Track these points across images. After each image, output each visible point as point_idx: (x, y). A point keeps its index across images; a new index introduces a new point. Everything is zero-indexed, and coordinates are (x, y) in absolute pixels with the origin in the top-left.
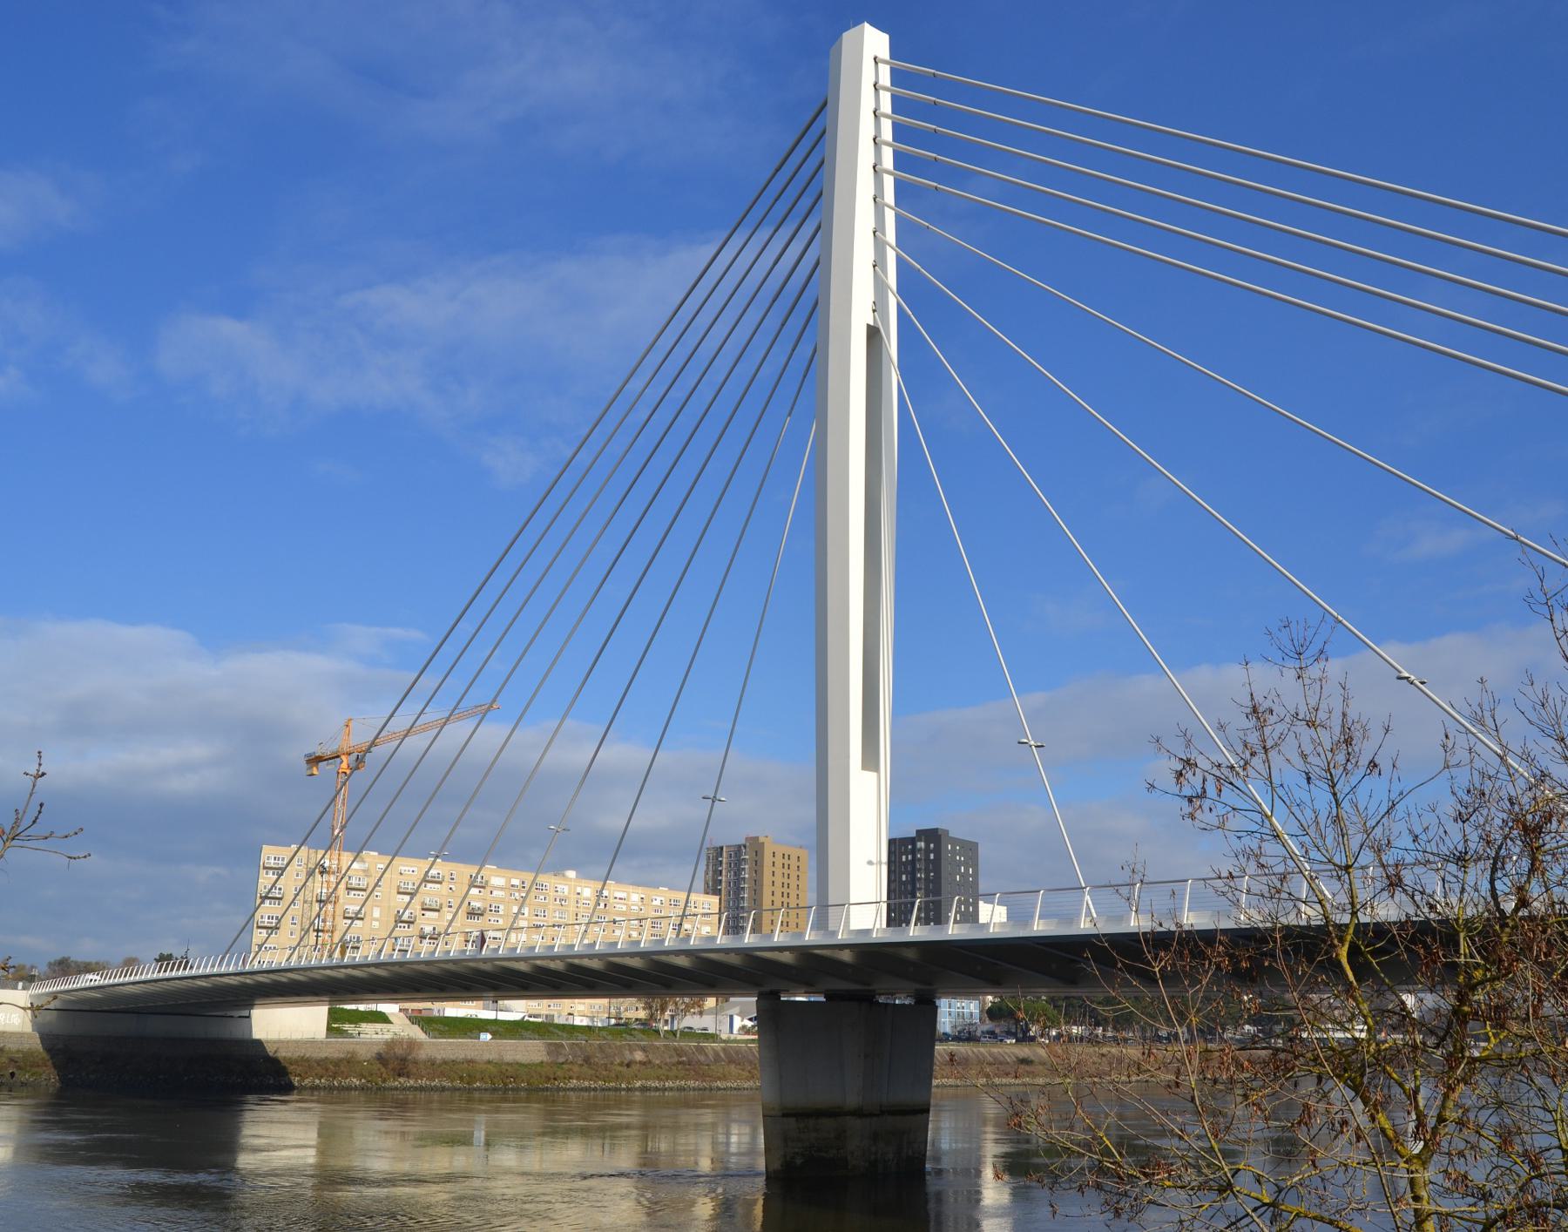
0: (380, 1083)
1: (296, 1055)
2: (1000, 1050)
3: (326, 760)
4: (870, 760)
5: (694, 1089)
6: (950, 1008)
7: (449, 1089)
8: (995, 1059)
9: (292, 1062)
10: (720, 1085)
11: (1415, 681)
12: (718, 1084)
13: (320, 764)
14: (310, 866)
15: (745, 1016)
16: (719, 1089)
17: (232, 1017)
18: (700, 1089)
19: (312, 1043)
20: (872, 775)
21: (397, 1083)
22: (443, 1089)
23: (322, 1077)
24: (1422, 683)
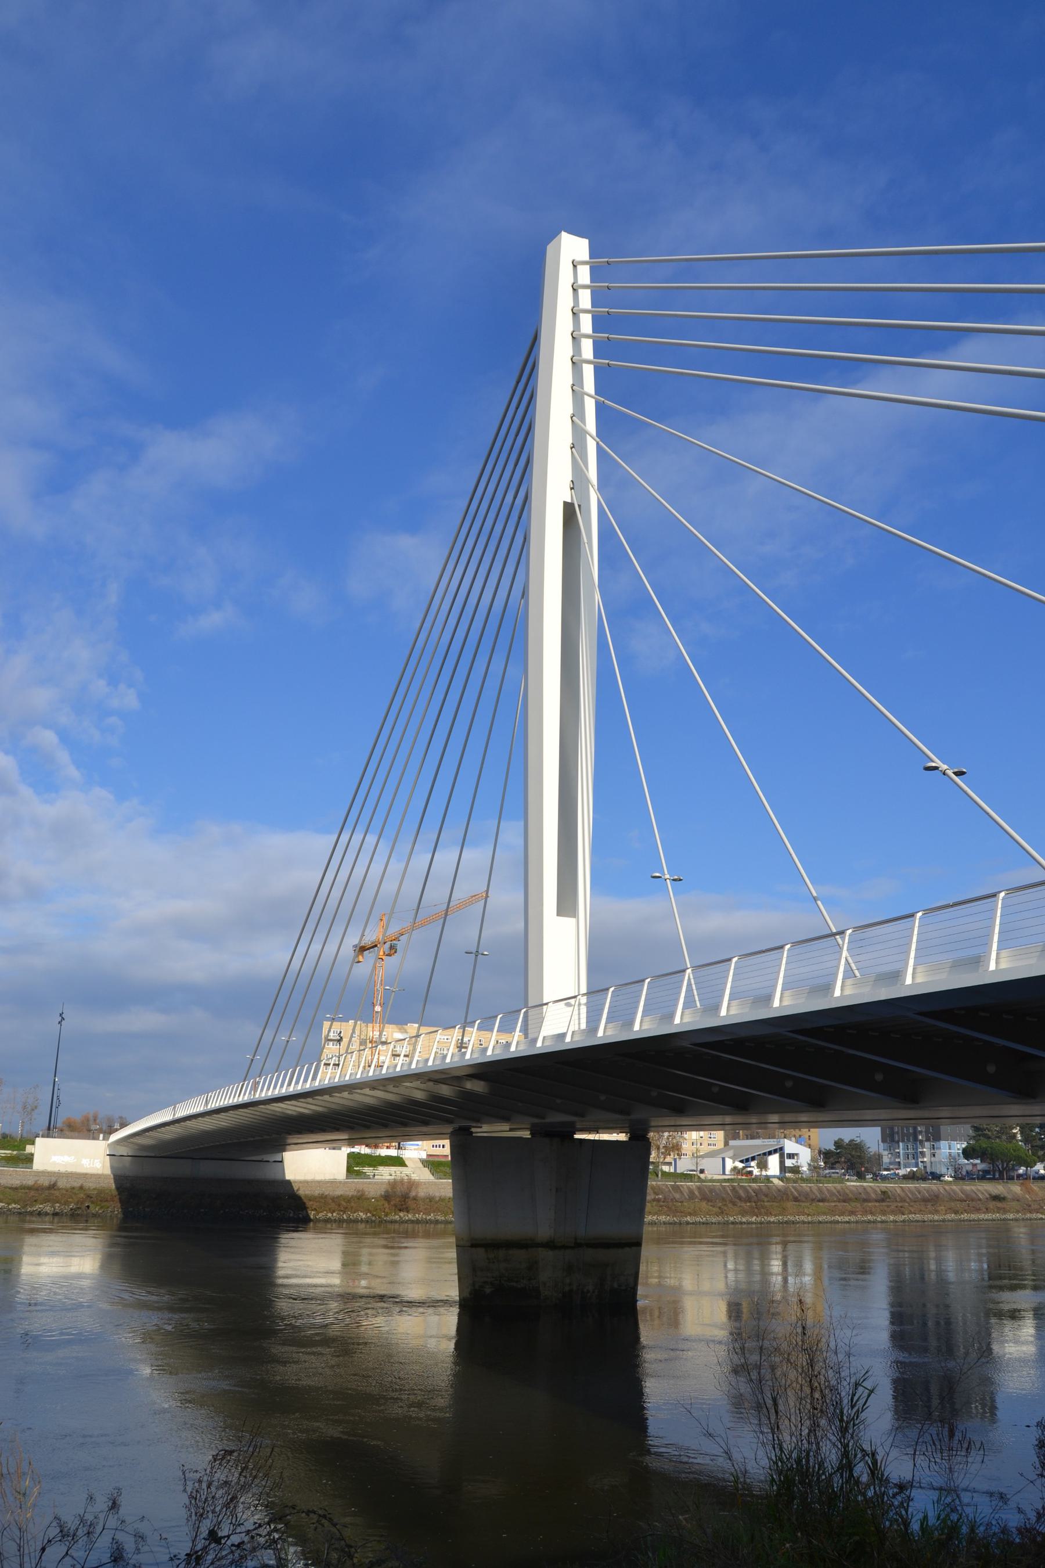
0: (383, 1217)
1: (317, 1193)
2: (973, 1188)
3: (368, 949)
4: (566, 905)
5: (665, 1223)
6: (950, 1149)
7: (442, 1222)
8: (967, 1196)
9: (312, 1198)
10: (689, 1220)
11: (948, 772)
12: (689, 1219)
13: (365, 952)
14: (362, 1037)
15: (737, 1159)
16: (688, 1223)
17: (268, 1161)
18: (671, 1224)
19: (333, 1183)
20: (570, 921)
21: (397, 1217)
22: (437, 1222)
23: (334, 1211)
24: (959, 774)
